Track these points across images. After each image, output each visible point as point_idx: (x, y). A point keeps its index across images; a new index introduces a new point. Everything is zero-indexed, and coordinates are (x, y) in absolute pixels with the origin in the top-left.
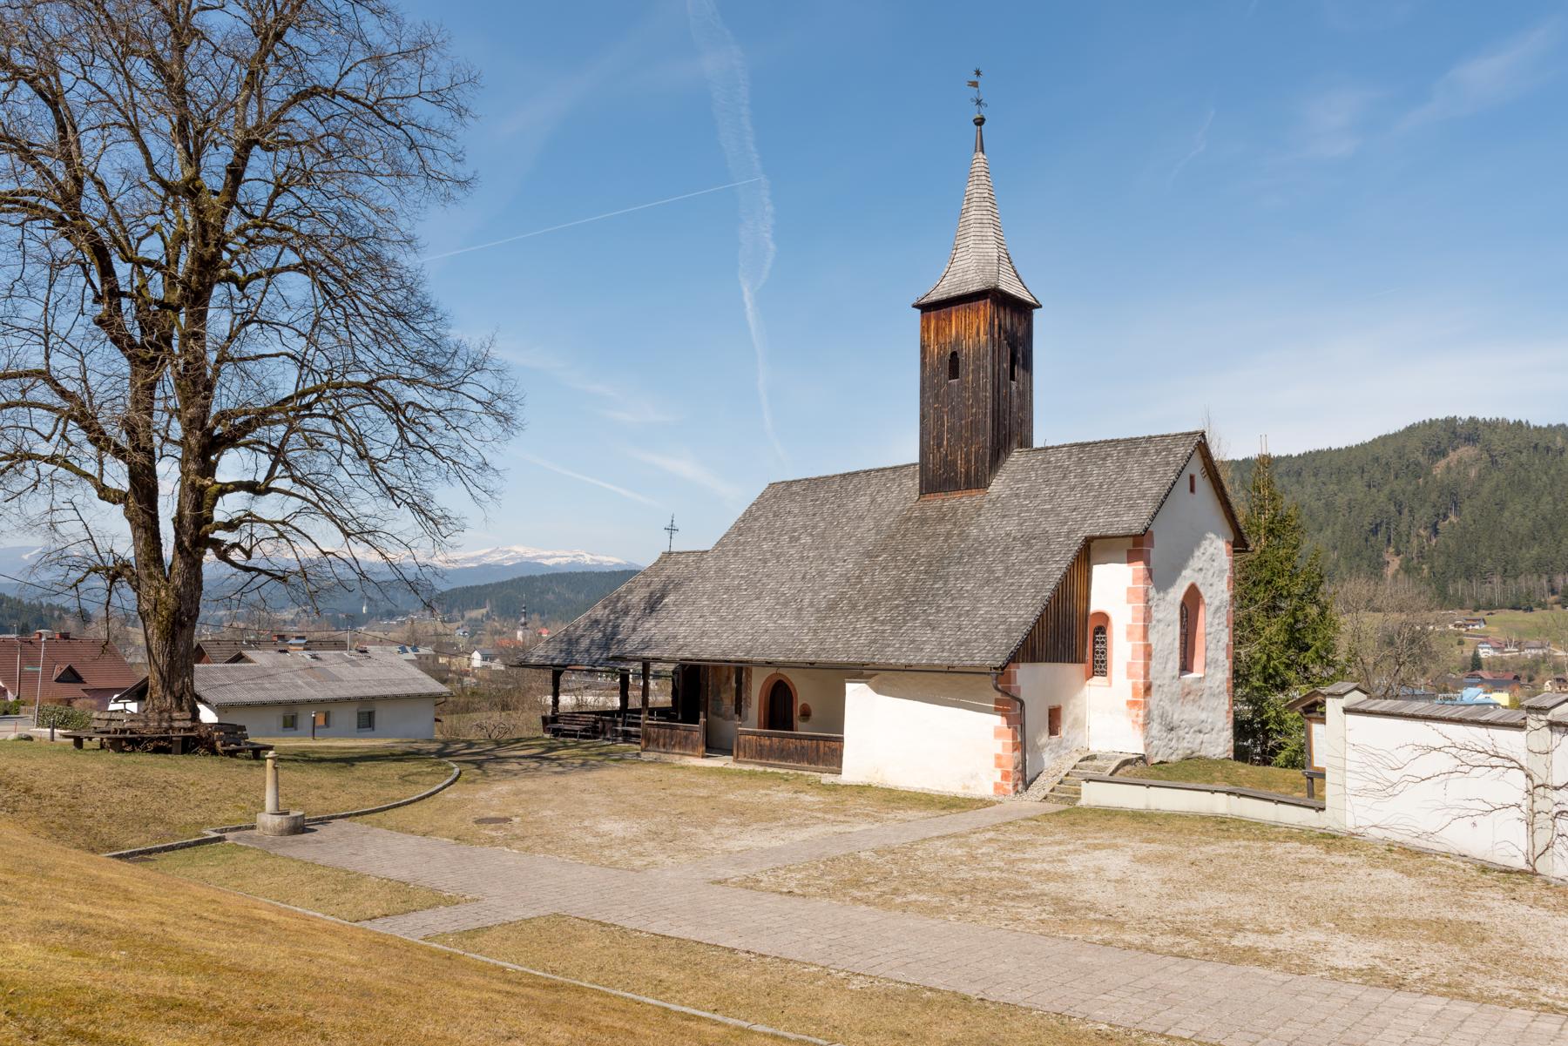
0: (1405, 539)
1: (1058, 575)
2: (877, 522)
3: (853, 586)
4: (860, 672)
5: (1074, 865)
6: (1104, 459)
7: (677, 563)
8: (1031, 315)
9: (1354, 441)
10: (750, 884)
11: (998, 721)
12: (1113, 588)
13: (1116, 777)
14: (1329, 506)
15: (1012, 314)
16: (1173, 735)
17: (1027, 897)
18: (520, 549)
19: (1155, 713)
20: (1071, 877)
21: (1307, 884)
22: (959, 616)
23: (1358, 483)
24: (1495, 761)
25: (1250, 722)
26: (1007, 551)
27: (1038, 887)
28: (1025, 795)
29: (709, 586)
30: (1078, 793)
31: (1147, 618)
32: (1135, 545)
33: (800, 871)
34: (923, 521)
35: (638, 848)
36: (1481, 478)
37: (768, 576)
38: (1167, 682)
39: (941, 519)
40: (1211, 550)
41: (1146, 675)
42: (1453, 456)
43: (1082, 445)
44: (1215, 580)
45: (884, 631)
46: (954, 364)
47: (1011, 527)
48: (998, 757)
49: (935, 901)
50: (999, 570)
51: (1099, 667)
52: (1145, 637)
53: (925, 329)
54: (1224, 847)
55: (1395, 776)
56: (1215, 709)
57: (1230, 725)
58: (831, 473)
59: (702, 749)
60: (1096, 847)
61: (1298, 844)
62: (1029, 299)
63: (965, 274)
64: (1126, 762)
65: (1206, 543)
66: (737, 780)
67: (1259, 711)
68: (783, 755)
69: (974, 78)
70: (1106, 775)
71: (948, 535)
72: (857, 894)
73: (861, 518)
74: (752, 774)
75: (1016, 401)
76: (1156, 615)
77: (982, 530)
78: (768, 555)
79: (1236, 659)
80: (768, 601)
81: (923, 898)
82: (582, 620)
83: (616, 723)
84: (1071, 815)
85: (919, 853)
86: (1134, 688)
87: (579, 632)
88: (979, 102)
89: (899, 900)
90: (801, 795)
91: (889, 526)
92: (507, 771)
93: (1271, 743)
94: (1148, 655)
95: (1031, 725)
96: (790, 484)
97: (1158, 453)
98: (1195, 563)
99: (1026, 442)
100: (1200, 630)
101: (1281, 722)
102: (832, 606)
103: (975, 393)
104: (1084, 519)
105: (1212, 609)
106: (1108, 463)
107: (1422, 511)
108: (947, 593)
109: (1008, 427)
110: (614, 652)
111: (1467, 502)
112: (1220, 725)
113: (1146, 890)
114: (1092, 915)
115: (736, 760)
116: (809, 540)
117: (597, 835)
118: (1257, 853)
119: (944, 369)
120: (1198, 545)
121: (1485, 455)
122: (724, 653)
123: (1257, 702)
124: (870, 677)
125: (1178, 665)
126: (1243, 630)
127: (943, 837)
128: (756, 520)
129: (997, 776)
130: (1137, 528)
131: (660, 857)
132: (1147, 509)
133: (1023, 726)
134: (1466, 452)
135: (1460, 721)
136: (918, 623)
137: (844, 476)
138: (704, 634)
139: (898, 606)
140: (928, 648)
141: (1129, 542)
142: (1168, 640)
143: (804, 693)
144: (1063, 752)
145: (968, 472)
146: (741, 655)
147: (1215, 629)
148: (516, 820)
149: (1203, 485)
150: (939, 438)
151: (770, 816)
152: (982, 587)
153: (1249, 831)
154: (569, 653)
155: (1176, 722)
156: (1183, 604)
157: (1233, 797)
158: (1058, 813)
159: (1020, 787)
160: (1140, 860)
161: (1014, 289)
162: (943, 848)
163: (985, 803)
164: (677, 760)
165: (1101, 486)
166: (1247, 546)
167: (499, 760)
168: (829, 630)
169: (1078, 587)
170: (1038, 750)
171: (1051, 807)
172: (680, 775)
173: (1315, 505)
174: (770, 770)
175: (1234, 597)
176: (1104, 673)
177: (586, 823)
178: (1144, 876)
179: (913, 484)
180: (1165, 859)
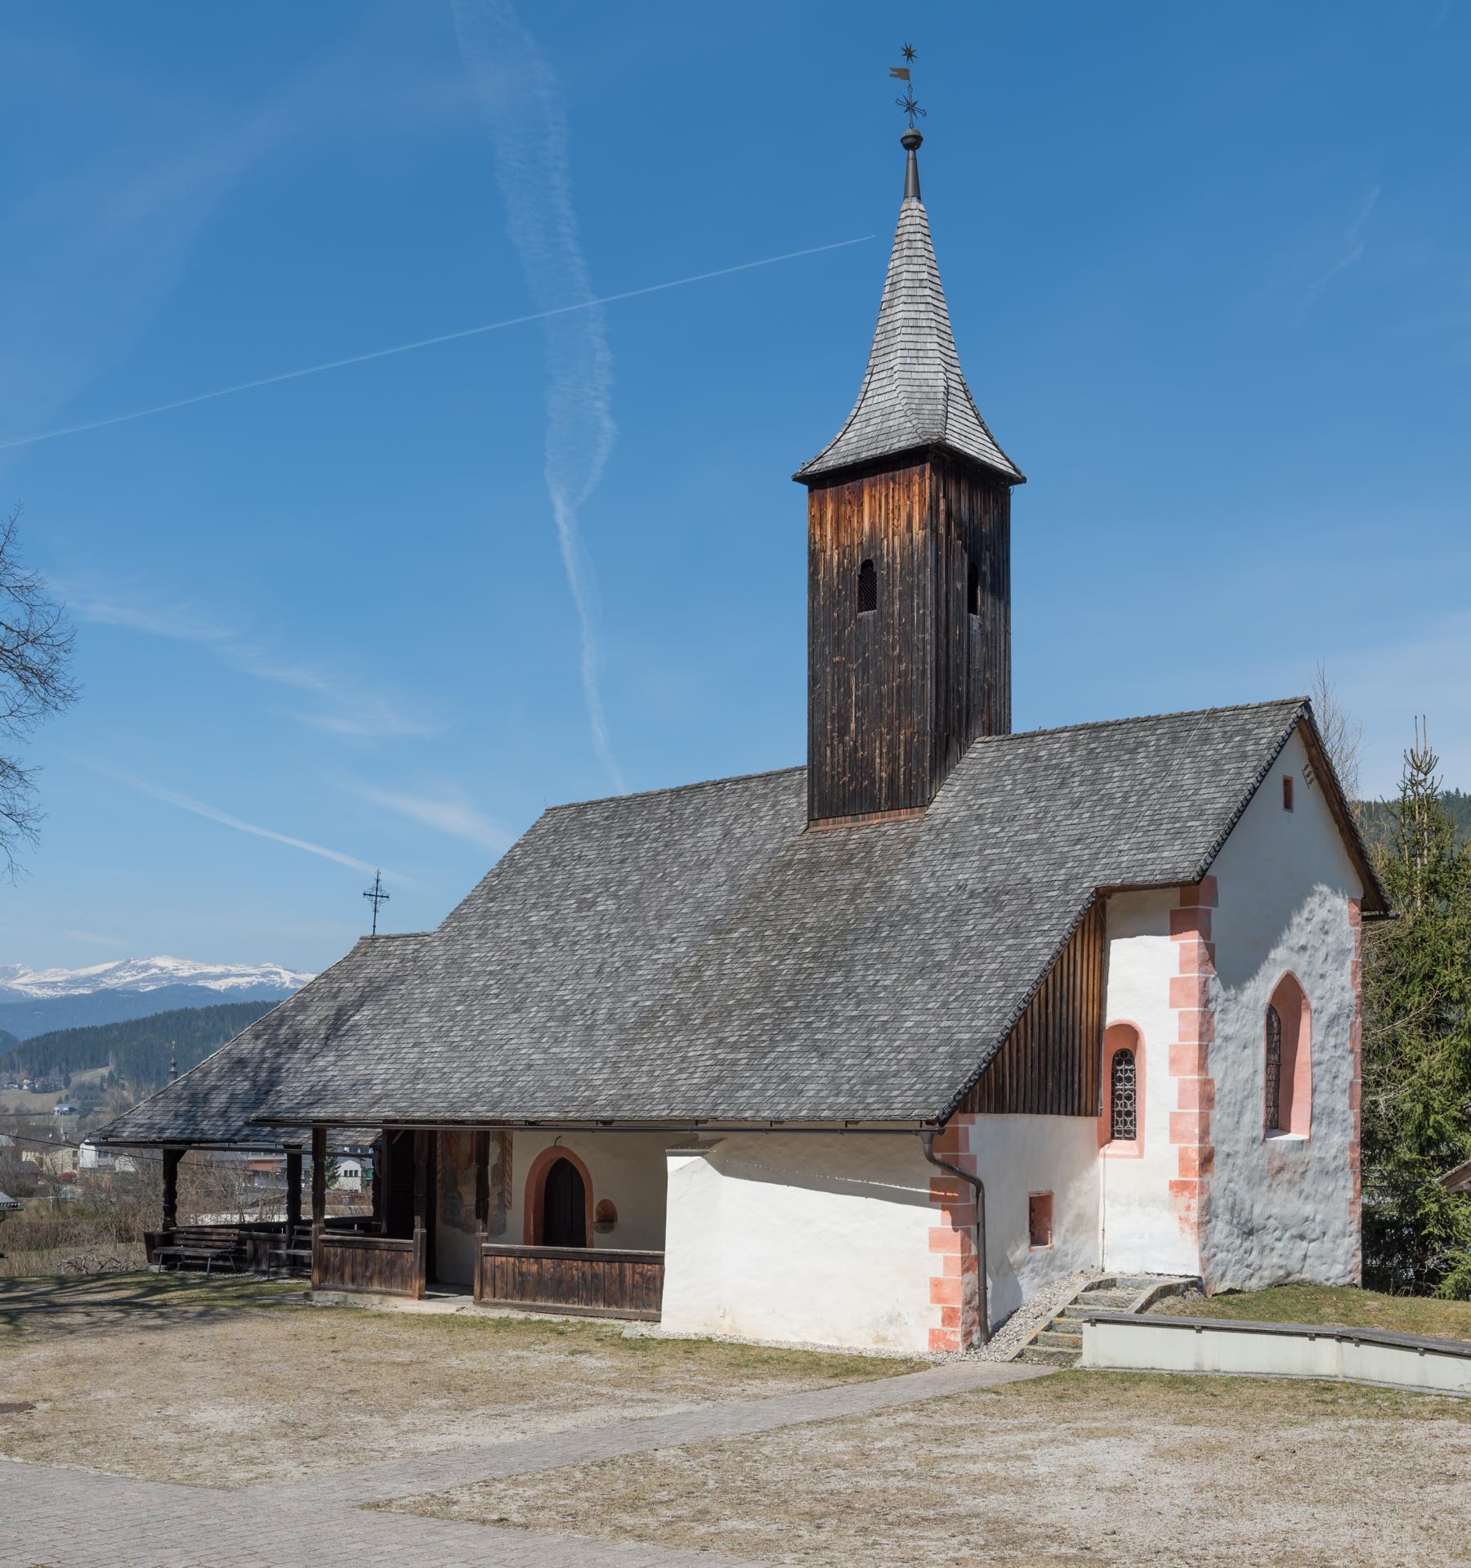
1: (1046, 956)
2: (732, 872)
3: (684, 985)
4: (690, 1134)
5: (1043, 1465)
6: (1133, 751)
7: (386, 955)
8: (1007, 494)
10: (436, 1509)
11: (936, 1218)
12: (1147, 980)
13: (1148, 1315)
15: (972, 496)
16: (1253, 1242)
17: (941, 1521)
18: (168, 963)
19: (1221, 1204)
20: (1032, 1484)
21: (1458, 1488)
22: (870, 1031)
25: (1396, 1224)
26: (957, 916)
27: (967, 1503)
28: (984, 1352)
29: (432, 991)
30: (1077, 1345)
31: (1206, 1032)
32: (1184, 901)
33: (534, 1483)
34: (813, 867)
35: (253, 1451)
37: (537, 970)
38: (1241, 1147)
39: (845, 864)
40: (1321, 914)
41: (1205, 1133)
43: (1096, 728)
44: (1329, 968)
45: (735, 1062)
46: (867, 581)
47: (967, 873)
48: (936, 1284)
49: (770, 1530)
50: (943, 949)
52: (1203, 1066)
53: (817, 520)
54: (1322, 1430)
56: (1328, 1198)
57: (1356, 1226)
58: (656, 788)
59: (418, 1283)
60: (1091, 1434)
61: (1455, 1422)
62: (1004, 466)
63: (885, 416)
64: (1167, 1291)
65: (1313, 902)
66: (472, 1335)
67: (1410, 1204)
68: (561, 1290)
69: (902, 63)
70: (1130, 1311)
71: (856, 891)
72: (627, 1520)
73: (705, 864)
74: (503, 1325)
75: (979, 651)
76: (1224, 1027)
77: (916, 880)
78: (539, 934)
79: (1369, 1114)
80: (535, 1014)
81: (751, 1525)
82: (215, 1059)
83: (276, 1244)
84: (1061, 1378)
85: (766, 1450)
87: (211, 1081)
88: (911, 107)
89: (701, 1530)
90: (582, 1359)
91: (753, 878)
92: (58, 1327)
93: (1431, 1263)
94: (1207, 1100)
95: (1005, 1225)
96: (581, 808)
97: (1227, 738)
98: (1296, 935)
99: (998, 725)
100: (1303, 1056)
101: (1449, 1223)
102: (647, 1021)
103: (906, 638)
104: (1095, 857)
105: (1324, 1019)
108: (849, 992)
109: (965, 699)
110: (263, 1112)
112: (1337, 1226)
113: (1159, 1502)
114: (1054, 1549)
115: (480, 1302)
116: (611, 905)
117: (186, 1429)
118: (1378, 1438)
119: (850, 592)
120: (1300, 907)
123: (1406, 1192)
124: (710, 1144)
125: (1262, 1120)
126: (1379, 1059)
127: (820, 1423)
128: (520, 872)
129: (935, 1319)
130: (1187, 870)
131: (287, 1465)
132: (1204, 836)
133: (981, 1226)
136: (795, 1046)
137: (677, 792)
138: (419, 1074)
139: (762, 1017)
140: (811, 1089)
142: (1245, 1073)
143: (604, 1181)
144: (1055, 1275)
145: (892, 780)
146: (481, 1111)
147: (1327, 1056)
148: (42, 1406)
149: (1307, 795)
150: (842, 718)
151: (521, 1393)
152: (910, 980)
153: (1372, 1402)
154: (191, 1118)
155: (1257, 1221)
156: (1271, 1011)
157: (1347, 1346)
158: (1037, 1381)
159: (975, 1338)
160: (1161, 1454)
161: (976, 446)
162: (813, 1442)
163: (911, 1365)
164: (373, 1303)
165: (1125, 798)
166: (1386, 908)
167: (53, 1308)
168: (640, 1062)
169: (1083, 979)
170: (1009, 1271)
171: (1028, 1370)
172: (372, 1328)
174: (535, 1317)
175: (1365, 1002)
176: (1130, 1135)
177: (171, 1411)
178: (1165, 1480)
179: (797, 803)
180: (1207, 1451)
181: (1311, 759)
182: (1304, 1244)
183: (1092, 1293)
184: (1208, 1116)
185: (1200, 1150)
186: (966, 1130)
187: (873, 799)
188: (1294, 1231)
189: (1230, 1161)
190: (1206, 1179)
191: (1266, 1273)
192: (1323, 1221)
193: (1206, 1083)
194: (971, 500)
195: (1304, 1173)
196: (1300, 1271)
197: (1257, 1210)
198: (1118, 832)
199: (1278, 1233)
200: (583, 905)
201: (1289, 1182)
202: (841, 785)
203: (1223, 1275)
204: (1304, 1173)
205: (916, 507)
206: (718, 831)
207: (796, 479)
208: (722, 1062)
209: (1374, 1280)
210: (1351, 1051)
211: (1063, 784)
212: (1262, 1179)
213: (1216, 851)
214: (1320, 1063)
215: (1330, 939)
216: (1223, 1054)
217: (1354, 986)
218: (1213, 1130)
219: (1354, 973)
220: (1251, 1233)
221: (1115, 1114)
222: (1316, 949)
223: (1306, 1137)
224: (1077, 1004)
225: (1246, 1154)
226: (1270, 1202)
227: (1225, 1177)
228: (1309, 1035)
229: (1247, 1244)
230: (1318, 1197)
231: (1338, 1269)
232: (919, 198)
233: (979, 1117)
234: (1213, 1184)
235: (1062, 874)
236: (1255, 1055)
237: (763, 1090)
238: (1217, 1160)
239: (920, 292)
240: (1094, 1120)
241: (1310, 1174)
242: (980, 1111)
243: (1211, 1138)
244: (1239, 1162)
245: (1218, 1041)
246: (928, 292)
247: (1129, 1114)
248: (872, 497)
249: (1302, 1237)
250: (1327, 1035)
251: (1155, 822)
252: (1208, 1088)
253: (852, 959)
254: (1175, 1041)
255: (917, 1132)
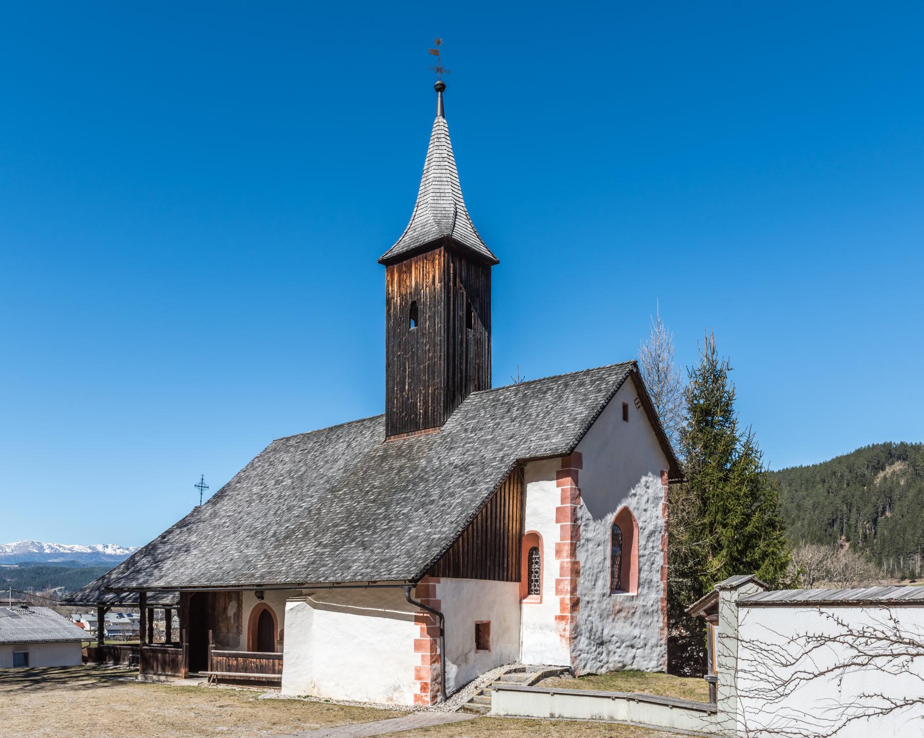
0: (853, 529)
1: (485, 494)
6: (545, 393)
9: (818, 461)
12: (544, 506)
14: (799, 507)
16: (603, 649)
22: (391, 536)
23: (820, 489)
24: (898, 648)
36: (908, 485)
38: (596, 598)
39: (399, 456)
42: (889, 470)
45: (323, 554)
46: (413, 310)
51: (532, 587)
52: (573, 553)
55: (785, 673)
56: (648, 626)
62: (488, 254)
70: (524, 685)
71: (401, 469)
73: (336, 461)
75: (472, 348)
76: (584, 534)
78: (255, 497)
86: (562, 602)
94: (576, 571)
96: (288, 439)
97: (593, 382)
99: (483, 385)
104: (518, 445)
105: (646, 532)
106: (548, 395)
107: (866, 509)
111: (898, 503)
112: (653, 641)
116: (290, 481)
121: (911, 469)
122: (191, 580)
129: (417, 689)
130: (563, 448)
134: (898, 466)
135: (858, 603)
141: (558, 463)
142: (599, 559)
145: (426, 412)
149: (636, 413)
155: (605, 638)
165: (538, 416)
169: (511, 507)
173: (790, 506)
181: (638, 395)
182: (634, 650)
183: (508, 675)
184: (576, 581)
185: (571, 599)
186: (434, 586)
187: (417, 423)
188: (628, 643)
189: (590, 605)
190: (574, 615)
191: (611, 665)
192: (645, 638)
193: (575, 563)
194: (468, 270)
195: (634, 613)
196: (632, 664)
197: (605, 632)
198: (532, 432)
199: (618, 644)
200: (278, 482)
201: (625, 617)
202: (401, 419)
203: (585, 666)
204: (634, 613)
205: (437, 272)
206: (345, 445)
207: (380, 262)
208: (317, 554)
209: (674, 669)
210: (662, 550)
211: (508, 411)
212: (608, 616)
213: (581, 438)
214: (644, 556)
215: (650, 491)
216: (585, 548)
217: (663, 516)
218: (579, 588)
219: (664, 510)
220: (602, 644)
221: (530, 581)
222: (642, 496)
223: (635, 594)
224: (506, 521)
225: (599, 602)
226: (614, 628)
227: (586, 614)
228: (639, 541)
229: (600, 650)
230: (642, 626)
231: (654, 663)
232: (444, 117)
233: (443, 580)
234: (579, 617)
235: (501, 454)
236: (605, 550)
237: (333, 566)
238: (581, 605)
239: (442, 163)
240: (517, 584)
241: (637, 614)
242: (444, 576)
243: (578, 593)
244: (595, 606)
245: (582, 541)
246: (446, 163)
247: (537, 581)
248: (416, 268)
249: (632, 646)
250: (648, 541)
251: (551, 426)
252: (576, 566)
253: (391, 500)
254: (559, 541)
255: (402, 586)
